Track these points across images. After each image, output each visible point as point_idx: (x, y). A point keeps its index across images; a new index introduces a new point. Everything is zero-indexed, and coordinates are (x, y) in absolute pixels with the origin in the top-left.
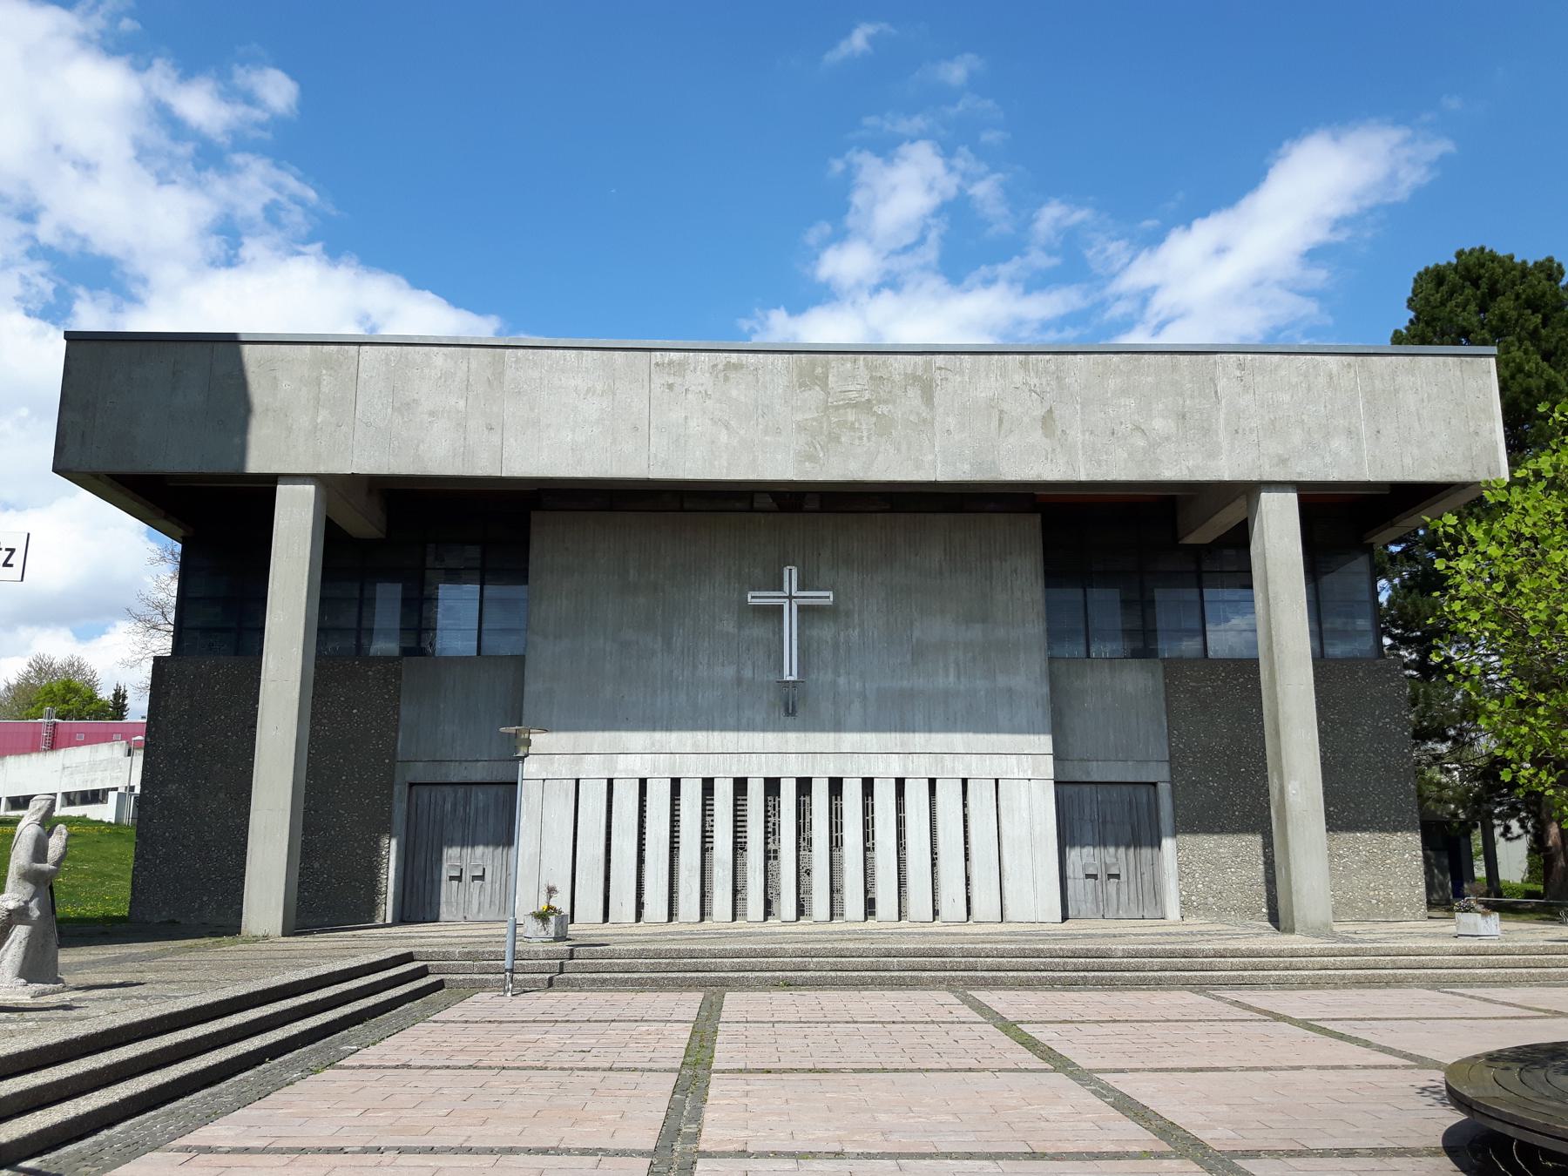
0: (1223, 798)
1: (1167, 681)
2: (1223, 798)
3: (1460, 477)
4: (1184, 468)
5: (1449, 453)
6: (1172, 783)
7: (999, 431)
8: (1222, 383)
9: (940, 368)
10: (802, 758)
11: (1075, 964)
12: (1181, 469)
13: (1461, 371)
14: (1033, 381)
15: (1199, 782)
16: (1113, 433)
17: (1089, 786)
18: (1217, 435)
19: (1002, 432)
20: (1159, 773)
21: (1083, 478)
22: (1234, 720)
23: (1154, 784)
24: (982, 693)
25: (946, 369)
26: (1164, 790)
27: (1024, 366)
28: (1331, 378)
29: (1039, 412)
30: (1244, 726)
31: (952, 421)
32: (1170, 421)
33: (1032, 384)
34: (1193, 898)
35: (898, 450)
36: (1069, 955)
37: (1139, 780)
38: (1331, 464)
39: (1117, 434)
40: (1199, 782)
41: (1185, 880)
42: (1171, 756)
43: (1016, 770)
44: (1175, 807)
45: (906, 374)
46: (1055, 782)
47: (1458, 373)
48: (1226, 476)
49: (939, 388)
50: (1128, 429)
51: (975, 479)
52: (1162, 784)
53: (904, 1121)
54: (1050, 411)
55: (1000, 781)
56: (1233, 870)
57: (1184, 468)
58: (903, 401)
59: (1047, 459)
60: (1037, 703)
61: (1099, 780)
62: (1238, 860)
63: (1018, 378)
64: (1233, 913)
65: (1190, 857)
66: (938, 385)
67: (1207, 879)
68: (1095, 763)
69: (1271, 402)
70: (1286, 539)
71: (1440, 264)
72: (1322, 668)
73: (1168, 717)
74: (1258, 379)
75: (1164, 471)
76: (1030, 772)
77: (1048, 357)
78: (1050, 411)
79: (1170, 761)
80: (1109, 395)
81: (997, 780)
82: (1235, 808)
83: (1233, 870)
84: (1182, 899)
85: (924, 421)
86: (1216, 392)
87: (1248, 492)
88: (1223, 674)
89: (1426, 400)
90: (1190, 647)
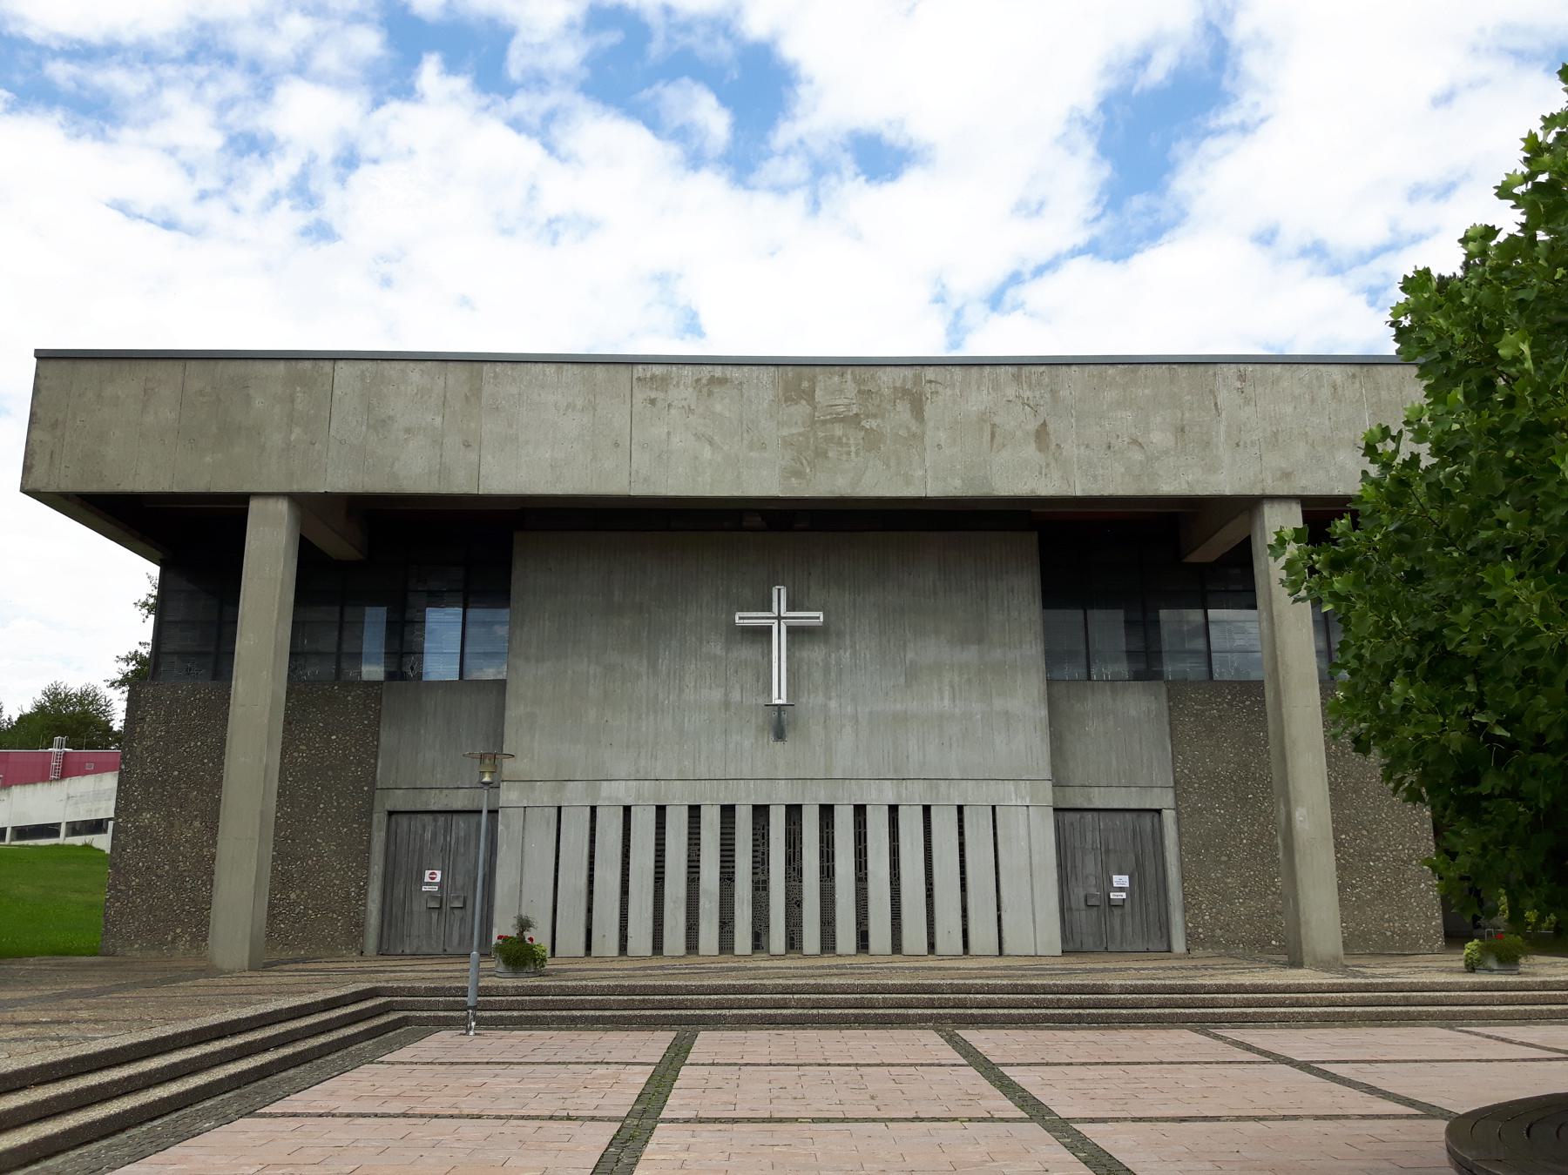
1: (1171, 704)
2: (1231, 825)
6: (1176, 809)
7: (992, 447)
9: (930, 382)
11: (1069, 1000)
12: (1179, 483)
14: (1027, 394)
16: (1109, 447)
17: (445, 815)
20: (1163, 799)
21: (1079, 493)
23: (1159, 811)
25: (936, 382)
27: (1017, 378)
29: (1032, 426)
30: (1251, 750)
31: (942, 436)
34: (1200, 930)
36: (1064, 991)
37: (1142, 807)
42: (1176, 782)
43: (1013, 797)
44: (1180, 835)
45: (894, 387)
54: (1044, 424)
56: (1241, 900)
59: (1041, 473)
61: (1101, 807)
63: (1011, 392)
64: (1241, 946)
66: (928, 398)
67: (1214, 910)
68: (1096, 789)
74: (1260, 390)
76: (1028, 799)
77: (1043, 368)
78: (1044, 424)
79: (1175, 787)
83: (1241, 900)
84: (1189, 931)
85: (914, 435)
86: (1216, 404)
87: (1248, 506)
88: (1229, 697)
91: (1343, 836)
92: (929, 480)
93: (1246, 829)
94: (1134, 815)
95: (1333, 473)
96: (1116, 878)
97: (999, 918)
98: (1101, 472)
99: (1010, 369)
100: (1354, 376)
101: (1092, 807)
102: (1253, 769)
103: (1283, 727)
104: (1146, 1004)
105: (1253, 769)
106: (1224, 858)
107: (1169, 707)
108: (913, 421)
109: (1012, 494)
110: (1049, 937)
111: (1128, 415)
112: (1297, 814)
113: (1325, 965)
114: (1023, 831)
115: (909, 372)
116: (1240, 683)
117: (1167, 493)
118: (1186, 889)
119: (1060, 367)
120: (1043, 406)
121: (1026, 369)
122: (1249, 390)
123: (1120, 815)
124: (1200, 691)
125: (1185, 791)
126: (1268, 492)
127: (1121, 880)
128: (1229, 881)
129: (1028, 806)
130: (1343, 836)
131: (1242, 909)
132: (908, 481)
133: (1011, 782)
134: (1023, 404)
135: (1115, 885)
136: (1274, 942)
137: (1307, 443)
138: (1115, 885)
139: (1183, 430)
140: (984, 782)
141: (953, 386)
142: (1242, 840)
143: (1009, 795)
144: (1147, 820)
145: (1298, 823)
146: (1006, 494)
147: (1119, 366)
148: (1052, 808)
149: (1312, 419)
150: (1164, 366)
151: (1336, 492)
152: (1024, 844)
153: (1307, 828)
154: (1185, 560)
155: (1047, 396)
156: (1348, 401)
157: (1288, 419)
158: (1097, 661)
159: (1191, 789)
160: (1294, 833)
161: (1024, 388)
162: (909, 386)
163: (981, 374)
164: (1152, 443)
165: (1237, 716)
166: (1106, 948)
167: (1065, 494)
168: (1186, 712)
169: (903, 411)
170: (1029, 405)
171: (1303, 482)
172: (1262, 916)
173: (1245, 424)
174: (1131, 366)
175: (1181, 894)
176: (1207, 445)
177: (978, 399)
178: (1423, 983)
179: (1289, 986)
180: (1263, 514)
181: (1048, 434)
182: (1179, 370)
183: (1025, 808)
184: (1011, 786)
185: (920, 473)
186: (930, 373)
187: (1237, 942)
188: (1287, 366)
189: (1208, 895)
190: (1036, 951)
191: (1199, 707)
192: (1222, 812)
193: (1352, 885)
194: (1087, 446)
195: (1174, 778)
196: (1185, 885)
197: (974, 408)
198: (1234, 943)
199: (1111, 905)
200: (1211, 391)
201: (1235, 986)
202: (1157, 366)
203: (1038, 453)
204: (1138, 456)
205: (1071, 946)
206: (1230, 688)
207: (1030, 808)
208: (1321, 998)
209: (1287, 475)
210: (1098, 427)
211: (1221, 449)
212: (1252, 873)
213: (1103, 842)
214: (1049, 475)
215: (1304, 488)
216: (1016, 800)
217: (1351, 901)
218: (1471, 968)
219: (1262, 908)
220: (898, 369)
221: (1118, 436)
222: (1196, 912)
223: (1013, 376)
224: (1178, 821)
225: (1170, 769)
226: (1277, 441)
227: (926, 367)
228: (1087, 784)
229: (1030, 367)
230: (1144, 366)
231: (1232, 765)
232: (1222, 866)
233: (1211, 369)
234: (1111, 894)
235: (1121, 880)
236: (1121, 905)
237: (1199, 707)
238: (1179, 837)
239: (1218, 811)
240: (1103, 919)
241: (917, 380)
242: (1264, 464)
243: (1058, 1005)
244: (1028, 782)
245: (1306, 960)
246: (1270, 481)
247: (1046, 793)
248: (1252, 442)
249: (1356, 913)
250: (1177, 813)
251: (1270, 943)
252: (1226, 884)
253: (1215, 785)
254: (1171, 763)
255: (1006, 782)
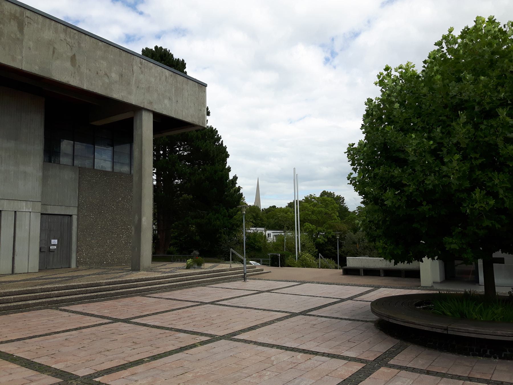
0: (95, 222)
1: (80, 176)
2: (95, 222)
3: (196, 123)
4: (120, 95)
5: (194, 114)
6: (78, 215)
7: (53, 57)
8: (135, 68)
9: (27, 17)
10: (30, 202)
11: (90, 290)
12: (119, 95)
13: (199, 89)
14: (69, 40)
15: (88, 216)
16: (97, 73)
17: (46, 215)
18: (132, 86)
19: (54, 57)
20: (73, 211)
21: (85, 88)
22: (102, 193)
23: (71, 216)
24: (12, 172)
25: (30, 18)
26: (75, 218)
27: (65, 31)
28: (166, 78)
29: (70, 54)
30: (105, 196)
31: (31, 44)
32: (117, 75)
33: (68, 41)
34: (82, 259)
35: (4, 49)
36: (85, 287)
37: (66, 214)
38: (164, 108)
39: (99, 74)
40: (88, 216)
41: (79, 253)
42: (79, 205)
43: (25, 208)
44: (78, 225)
45: (11, 13)
46: (42, 214)
47: (198, 89)
48: (134, 103)
49: (26, 26)
50: (103, 74)
51: (41, 74)
52: (75, 216)
53: (226, 377)
54: (74, 55)
55: (17, 212)
56: (96, 248)
57: (120, 95)
58: (8, 25)
59: (72, 75)
60: (37, 180)
61: (51, 213)
62: (98, 245)
63: (62, 36)
64: (94, 264)
65: (82, 244)
66: (26, 24)
67: (87, 252)
68: (49, 206)
69: (149, 80)
70: (149, 131)
71: (162, 47)
72: (130, 178)
73: (79, 190)
74: (146, 70)
75: (114, 94)
76: (31, 209)
77: (75, 32)
78: (74, 55)
79: (78, 207)
80: (97, 57)
81: (15, 212)
82: (99, 225)
83: (96, 248)
84: (78, 260)
85: (18, 39)
86: (133, 70)
87: (137, 110)
88: (100, 176)
89: (190, 95)
90: (87, 164)
91: (129, 226)
92: (24, 63)
93: (100, 223)
94: (62, 217)
95: (163, 106)
96: (52, 241)
97: (13, 258)
98: (94, 82)
99: (62, 26)
100: (171, 75)
101: (47, 213)
102: (104, 202)
103: (141, 190)
104: (116, 289)
105: (104, 202)
106: (92, 233)
107: (79, 177)
108: (18, 33)
109: (60, 80)
110: (34, 263)
111: (105, 64)
112: (143, 219)
113: (149, 270)
114: (27, 222)
115: (18, 8)
116: (103, 171)
117: (115, 98)
118: (78, 245)
119: (82, 34)
120: (75, 47)
121: (69, 29)
122: (143, 69)
123: (57, 217)
124: (90, 172)
125: (81, 208)
126: (145, 107)
127: (54, 242)
128: (93, 241)
129: (30, 212)
130: (129, 226)
131: (96, 251)
132: (14, 59)
133: (24, 202)
134: (67, 43)
135: (52, 243)
136: (105, 263)
137: (157, 93)
138: (52, 243)
139: (122, 76)
140: (12, 201)
141: (38, 24)
142: (98, 227)
143: (23, 207)
144: (66, 219)
145: (143, 222)
146: (57, 80)
147: (103, 43)
148: (40, 214)
149: (159, 86)
150: (118, 49)
151: (163, 113)
152: (27, 227)
153: (145, 224)
154: (91, 123)
155: (77, 44)
156: (169, 83)
157: (153, 83)
158: (54, 155)
159: (83, 208)
160: (142, 226)
161: (68, 37)
162: (18, 15)
163: (51, 24)
164: (112, 77)
165: (101, 183)
166: (46, 268)
167: (80, 86)
168: (85, 180)
169: (13, 27)
170: (69, 45)
171: (155, 107)
172: (102, 253)
173: (141, 80)
174: (108, 45)
175: (76, 246)
176: (129, 84)
177: (48, 34)
178: (188, 273)
179: (155, 278)
180: (142, 114)
181: (76, 60)
182: (123, 53)
183: (29, 213)
184: (24, 203)
185: (19, 57)
186: (28, 13)
187: (93, 263)
188: (154, 65)
189: (85, 247)
190: (28, 271)
191: (89, 178)
192: (93, 217)
193: (130, 242)
194: (90, 70)
195: (78, 204)
196: (78, 243)
197: (47, 37)
198: (92, 263)
199: (50, 250)
200: (132, 65)
201: (140, 279)
202: (116, 48)
203: (71, 66)
204: (107, 80)
205: (44, 266)
206: (100, 173)
207: (31, 213)
208: (166, 281)
209: (151, 103)
210: (94, 64)
211: (133, 87)
212: (100, 238)
213: (49, 227)
214: (75, 77)
215: (155, 109)
216: (26, 209)
217: (129, 248)
218: (188, 268)
219: (102, 251)
220: (13, 5)
221: (101, 70)
222: (81, 253)
223: (64, 29)
224: (78, 219)
225: (77, 201)
226: (149, 90)
227: (26, 10)
228: (46, 204)
229: (71, 29)
230: (111, 46)
231: (98, 200)
232: (91, 236)
233: (133, 57)
234: (51, 247)
235: (54, 242)
236: (53, 251)
237: (89, 178)
238: (78, 226)
239: (92, 216)
240: (46, 257)
241: (22, 14)
242: (145, 97)
243: (86, 292)
244: (31, 202)
245: (141, 268)
246: (146, 103)
247: (39, 207)
248: (142, 88)
249: (130, 252)
250: (78, 217)
251: (104, 263)
252: (92, 242)
253: (92, 207)
254: (77, 198)
255: (22, 201)
